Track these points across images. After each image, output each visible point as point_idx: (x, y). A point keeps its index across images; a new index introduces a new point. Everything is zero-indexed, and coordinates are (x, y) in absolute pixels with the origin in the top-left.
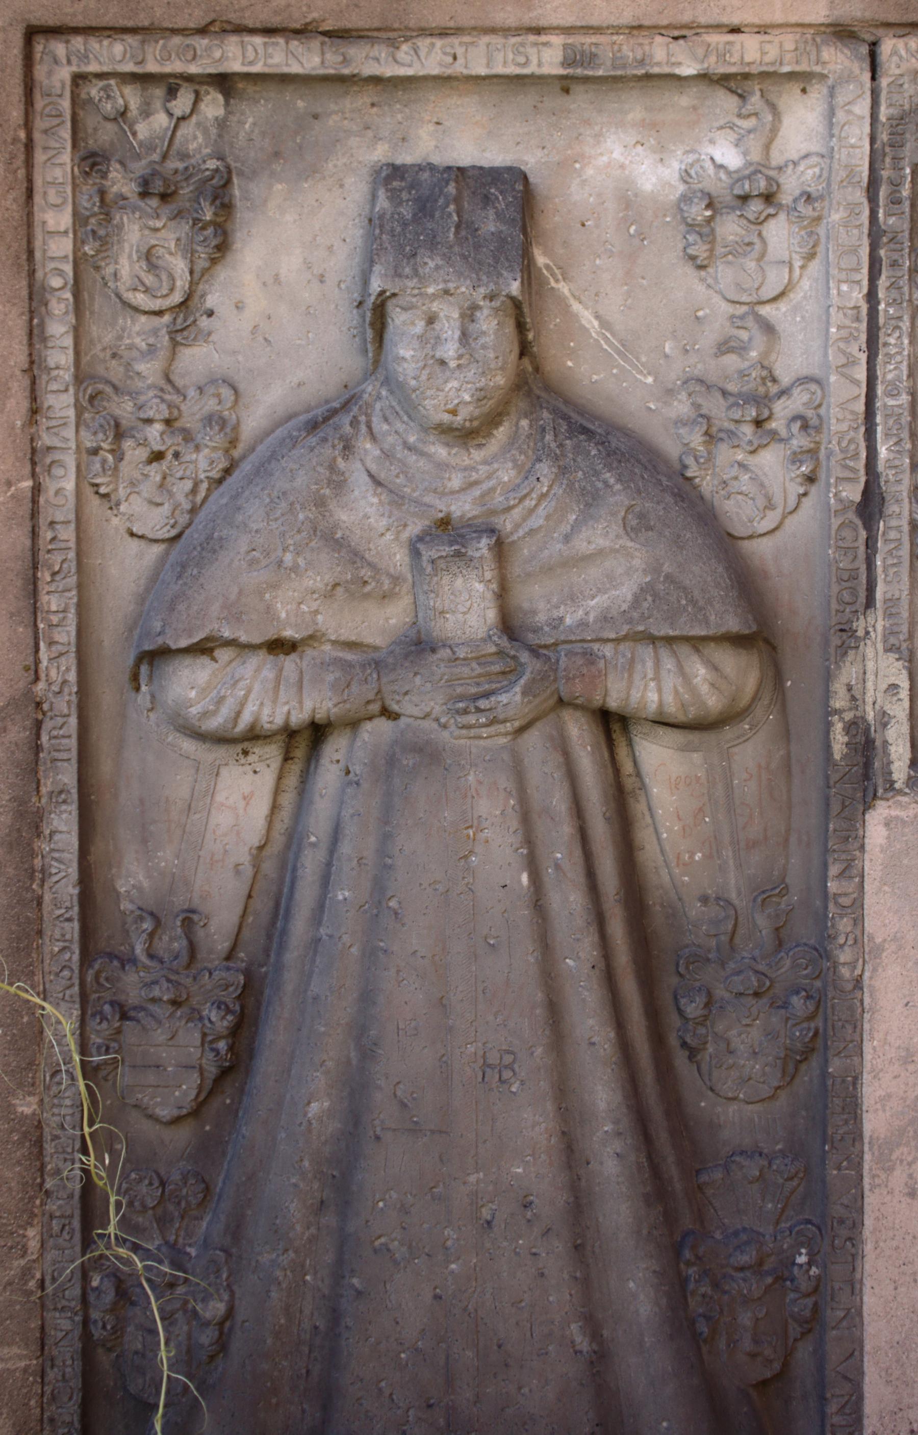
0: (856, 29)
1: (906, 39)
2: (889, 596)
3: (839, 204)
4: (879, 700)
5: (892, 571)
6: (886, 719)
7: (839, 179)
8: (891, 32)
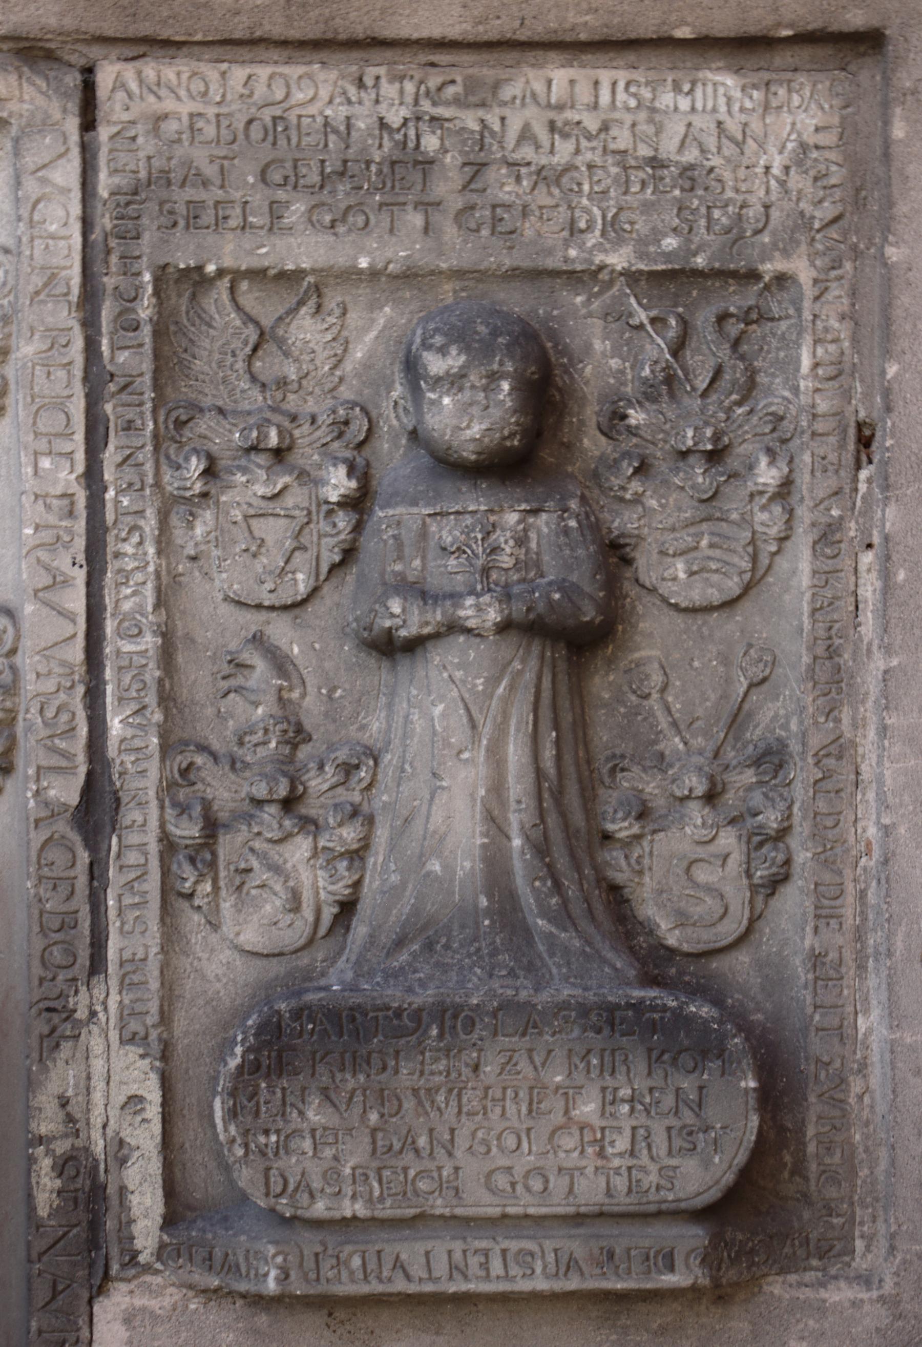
0: (52, 45)
1: (138, 64)
2: (127, 955)
3: (32, 330)
4: (112, 1122)
5: (131, 915)
6: (125, 1151)
7: (31, 289)
8: (115, 52)
